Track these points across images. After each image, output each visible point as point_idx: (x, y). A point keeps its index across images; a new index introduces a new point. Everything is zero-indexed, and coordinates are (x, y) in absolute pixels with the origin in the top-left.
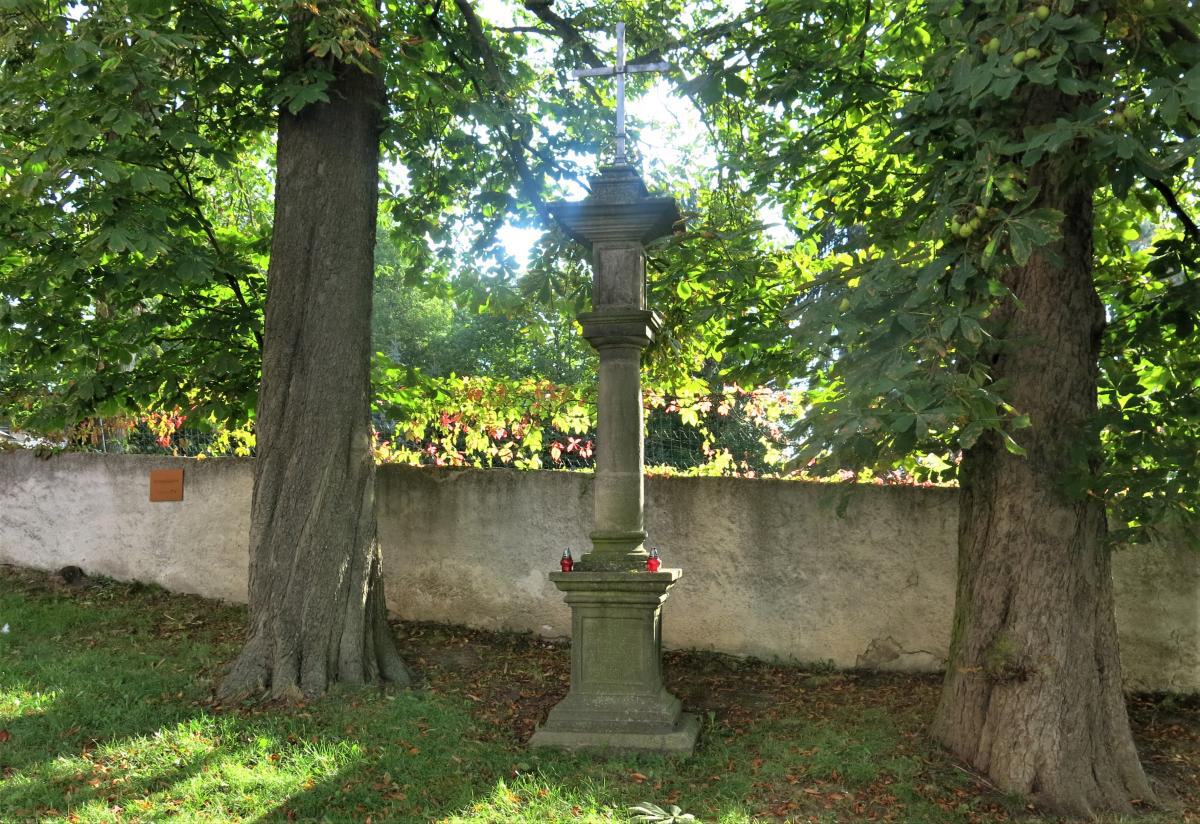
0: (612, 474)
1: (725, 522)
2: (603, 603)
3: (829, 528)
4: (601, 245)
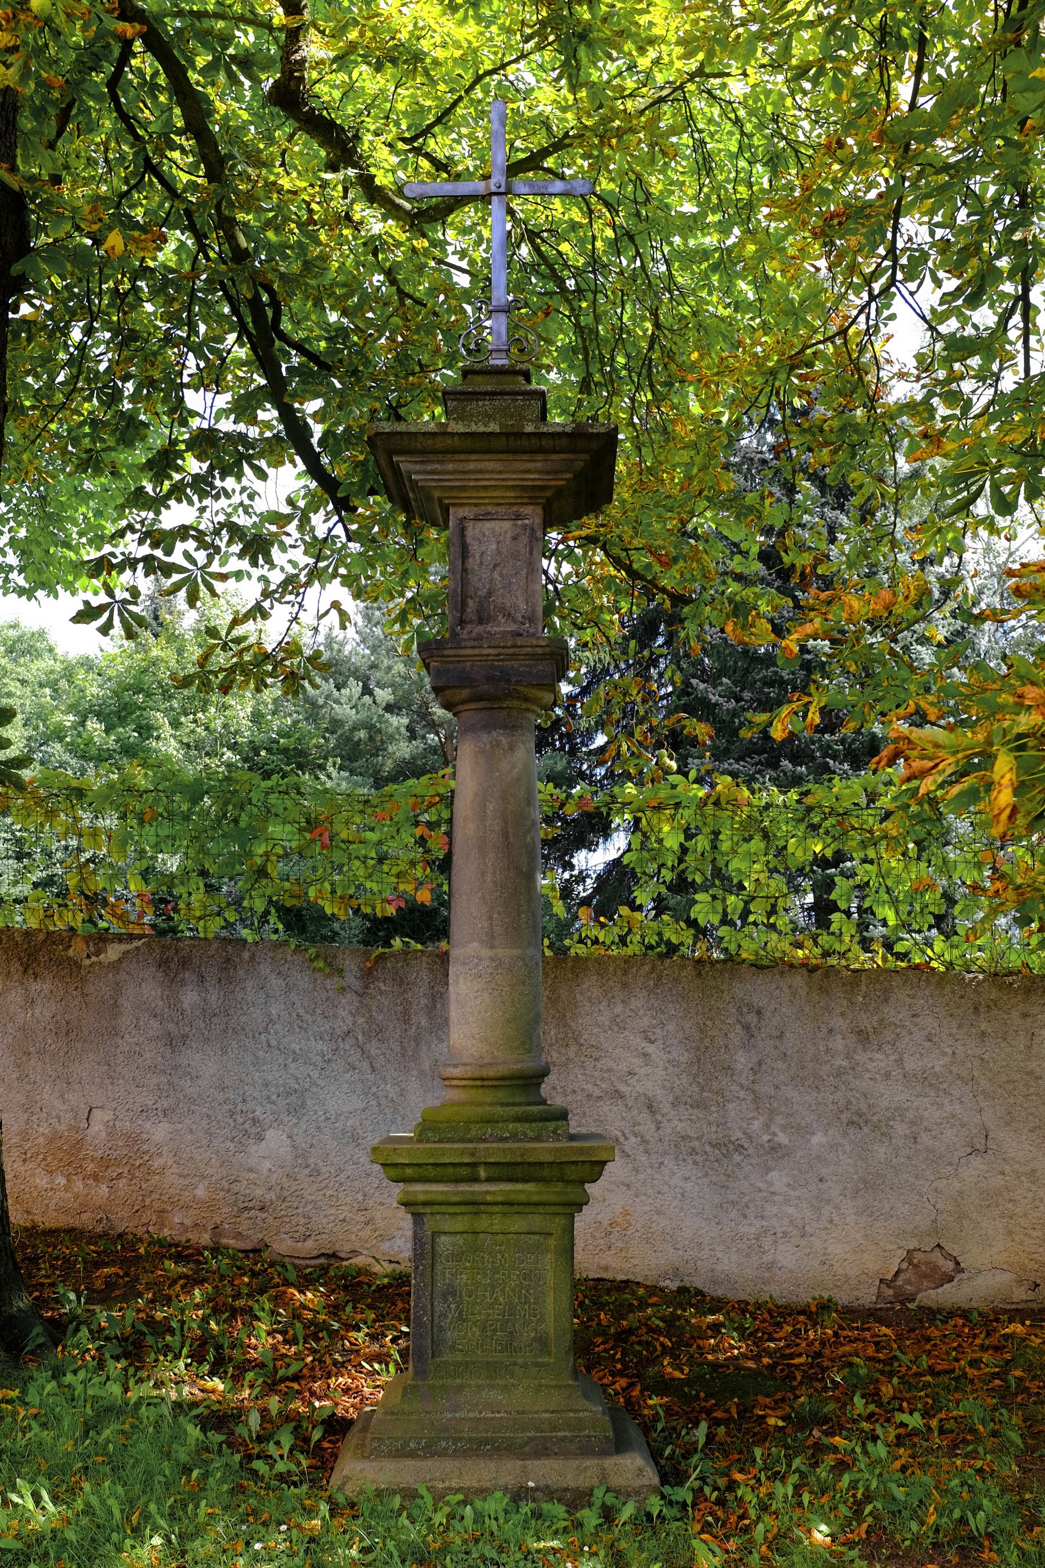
0: (486, 953)
1: (637, 1041)
2: (475, 1205)
3: (828, 1050)
4: (462, 512)
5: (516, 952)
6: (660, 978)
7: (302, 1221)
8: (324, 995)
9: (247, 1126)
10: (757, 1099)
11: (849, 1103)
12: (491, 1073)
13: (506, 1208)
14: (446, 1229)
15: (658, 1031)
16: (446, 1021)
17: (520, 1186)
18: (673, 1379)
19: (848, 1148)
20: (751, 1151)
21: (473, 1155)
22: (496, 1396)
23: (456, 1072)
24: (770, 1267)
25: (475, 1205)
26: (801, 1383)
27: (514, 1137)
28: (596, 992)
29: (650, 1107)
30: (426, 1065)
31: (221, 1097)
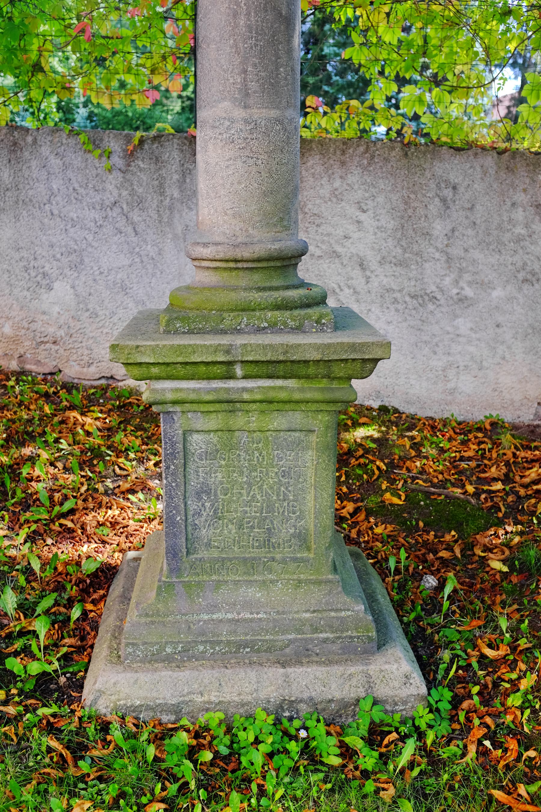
0: (239, 113)
1: (352, 211)
2: (230, 404)
3: (510, 220)
5: (274, 113)
6: (373, 157)
7: (86, 352)
8: (94, 172)
9: (39, 278)
10: (449, 259)
11: (525, 264)
12: (246, 254)
13: (264, 406)
14: (199, 427)
15: (369, 202)
16: (195, 193)
17: (279, 383)
18: (392, 505)
19: (521, 301)
20: (442, 302)
21: (228, 352)
22: (254, 593)
23: (206, 252)
24: (453, 391)
25: (230, 404)
26: (506, 516)
27: (273, 327)
28: (319, 169)
29: (361, 265)
30: (179, 229)
31: (17, 256)
